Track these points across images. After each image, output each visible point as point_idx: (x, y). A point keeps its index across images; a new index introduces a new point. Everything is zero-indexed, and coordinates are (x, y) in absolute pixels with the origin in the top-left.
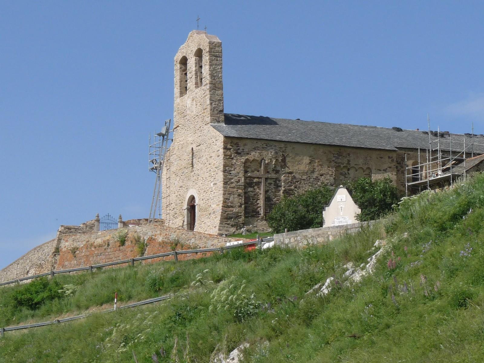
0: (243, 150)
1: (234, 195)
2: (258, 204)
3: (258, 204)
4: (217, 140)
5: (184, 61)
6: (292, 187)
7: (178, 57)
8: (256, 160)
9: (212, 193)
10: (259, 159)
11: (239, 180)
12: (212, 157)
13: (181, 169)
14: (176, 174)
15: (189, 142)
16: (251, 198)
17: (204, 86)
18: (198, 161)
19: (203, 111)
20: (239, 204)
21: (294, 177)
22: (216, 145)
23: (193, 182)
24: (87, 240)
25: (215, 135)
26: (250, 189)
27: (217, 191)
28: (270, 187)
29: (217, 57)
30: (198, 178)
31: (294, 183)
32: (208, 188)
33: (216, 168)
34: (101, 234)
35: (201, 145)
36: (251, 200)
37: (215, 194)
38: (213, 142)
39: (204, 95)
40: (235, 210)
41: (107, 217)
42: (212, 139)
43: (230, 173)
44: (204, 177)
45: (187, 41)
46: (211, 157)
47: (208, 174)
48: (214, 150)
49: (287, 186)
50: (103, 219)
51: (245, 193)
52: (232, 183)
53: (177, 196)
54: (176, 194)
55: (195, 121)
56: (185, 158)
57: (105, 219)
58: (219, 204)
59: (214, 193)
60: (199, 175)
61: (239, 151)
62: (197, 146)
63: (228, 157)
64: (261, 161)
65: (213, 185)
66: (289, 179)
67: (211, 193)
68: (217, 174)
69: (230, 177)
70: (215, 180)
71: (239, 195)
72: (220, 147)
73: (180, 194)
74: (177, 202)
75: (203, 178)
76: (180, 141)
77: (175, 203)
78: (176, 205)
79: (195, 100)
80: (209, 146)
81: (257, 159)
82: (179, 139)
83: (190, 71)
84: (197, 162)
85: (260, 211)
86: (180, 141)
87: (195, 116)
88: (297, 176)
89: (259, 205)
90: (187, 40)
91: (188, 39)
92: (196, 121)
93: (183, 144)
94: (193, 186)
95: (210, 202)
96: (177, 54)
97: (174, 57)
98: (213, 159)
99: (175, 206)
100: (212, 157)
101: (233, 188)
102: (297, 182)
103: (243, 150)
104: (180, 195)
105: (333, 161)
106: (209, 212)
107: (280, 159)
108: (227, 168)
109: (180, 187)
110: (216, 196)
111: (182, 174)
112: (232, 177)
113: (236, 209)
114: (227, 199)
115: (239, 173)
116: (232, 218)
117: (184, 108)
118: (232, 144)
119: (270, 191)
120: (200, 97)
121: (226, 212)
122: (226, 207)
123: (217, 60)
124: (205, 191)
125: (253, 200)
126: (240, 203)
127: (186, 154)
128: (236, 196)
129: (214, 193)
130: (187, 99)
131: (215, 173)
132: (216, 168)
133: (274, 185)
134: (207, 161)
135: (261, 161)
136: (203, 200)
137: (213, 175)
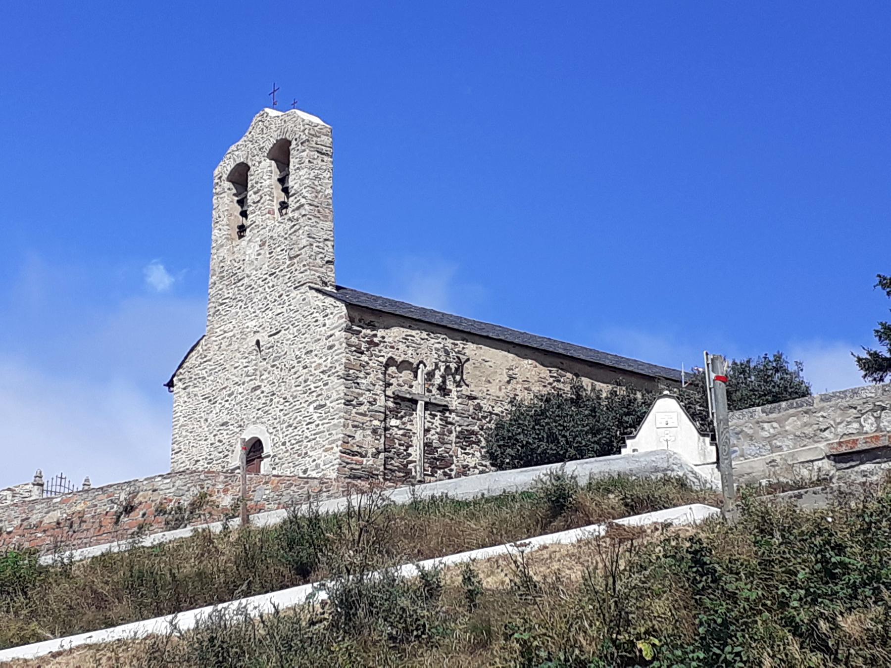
0: (383, 337)
1: (364, 429)
2: (410, 455)
3: (410, 455)
4: (327, 316)
5: (240, 177)
6: (476, 428)
7: (226, 167)
8: (408, 361)
9: (312, 426)
10: (415, 362)
11: (375, 400)
12: (311, 351)
13: (225, 388)
14: (210, 401)
15: (249, 330)
16: (396, 441)
17: (293, 211)
18: (273, 366)
19: (288, 262)
20: (374, 450)
21: (479, 408)
22: (324, 325)
23: (258, 410)
24: (24, 516)
25: (321, 304)
26: (394, 422)
27: (326, 421)
28: (433, 423)
29: (323, 154)
30: (271, 400)
31: (478, 420)
32: (299, 418)
33: (322, 372)
34: (60, 502)
35: (283, 332)
36: (397, 445)
37: (320, 427)
38: (316, 321)
39: (293, 230)
40: (368, 462)
41: (59, 480)
42: (314, 315)
43: (358, 384)
44: (288, 397)
45: (247, 134)
46: (309, 352)
47: (298, 388)
48: (319, 337)
49: (466, 424)
50: (50, 484)
51: (386, 429)
52: (361, 404)
53: (212, 444)
54: (209, 442)
55: (266, 286)
56: (236, 365)
57: (54, 483)
58: (332, 448)
59: (318, 425)
60: (274, 394)
61: (376, 340)
62: (270, 336)
63: (354, 349)
64: (418, 365)
65: (315, 408)
66: (469, 411)
67: (309, 426)
68: (325, 385)
69: (357, 390)
70: (319, 398)
71: (374, 431)
72: (336, 327)
73: (222, 439)
74: (212, 457)
75: (284, 399)
76: (225, 332)
77: (206, 458)
78: (208, 463)
79: (267, 244)
80: (303, 331)
81: (411, 360)
82: (222, 328)
83: (255, 189)
84: (270, 369)
85: (413, 470)
86: (225, 332)
87: (265, 277)
88: (486, 407)
89: (410, 458)
90: (250, 130)
91: (251, 128)
92: (270, 285)
93: (234, 336)
94: (258, 418)
95: (306, 447)
96: (221, 163)
97: (214, 170)
98: (316, 355)
99: (206, 465)
100: (311, 351)
101: (364, 415)
102: (485, 417)
103: (383, 337)
104: (220, 441)
106: (304, 468)
107: (453, 366)
108: (351, 372)
109: (222, 425)
110: (324, 432)
111: (227, 398)
112: (361, 391)
113: (368, 461)
114: (349, 436)
115: (374, 385)
117: (236, 264)
118: (361, 324)
119: (433, 432)
120: (283, 234)
121: (348, 463)
122: (349, 454)
123: (323, 161)
124: (290, 426)
125: (400, 445)
126: (376, 449)
127: (239, 355)
128: (369, 432)
129: (318, 425)
130: (249, 247)
131: (320, 383)
132: (322, 372)
133: (441, 419)
134: (299, 362)
135: (418, 365)
136: (284, 444)
137: (313, 389)
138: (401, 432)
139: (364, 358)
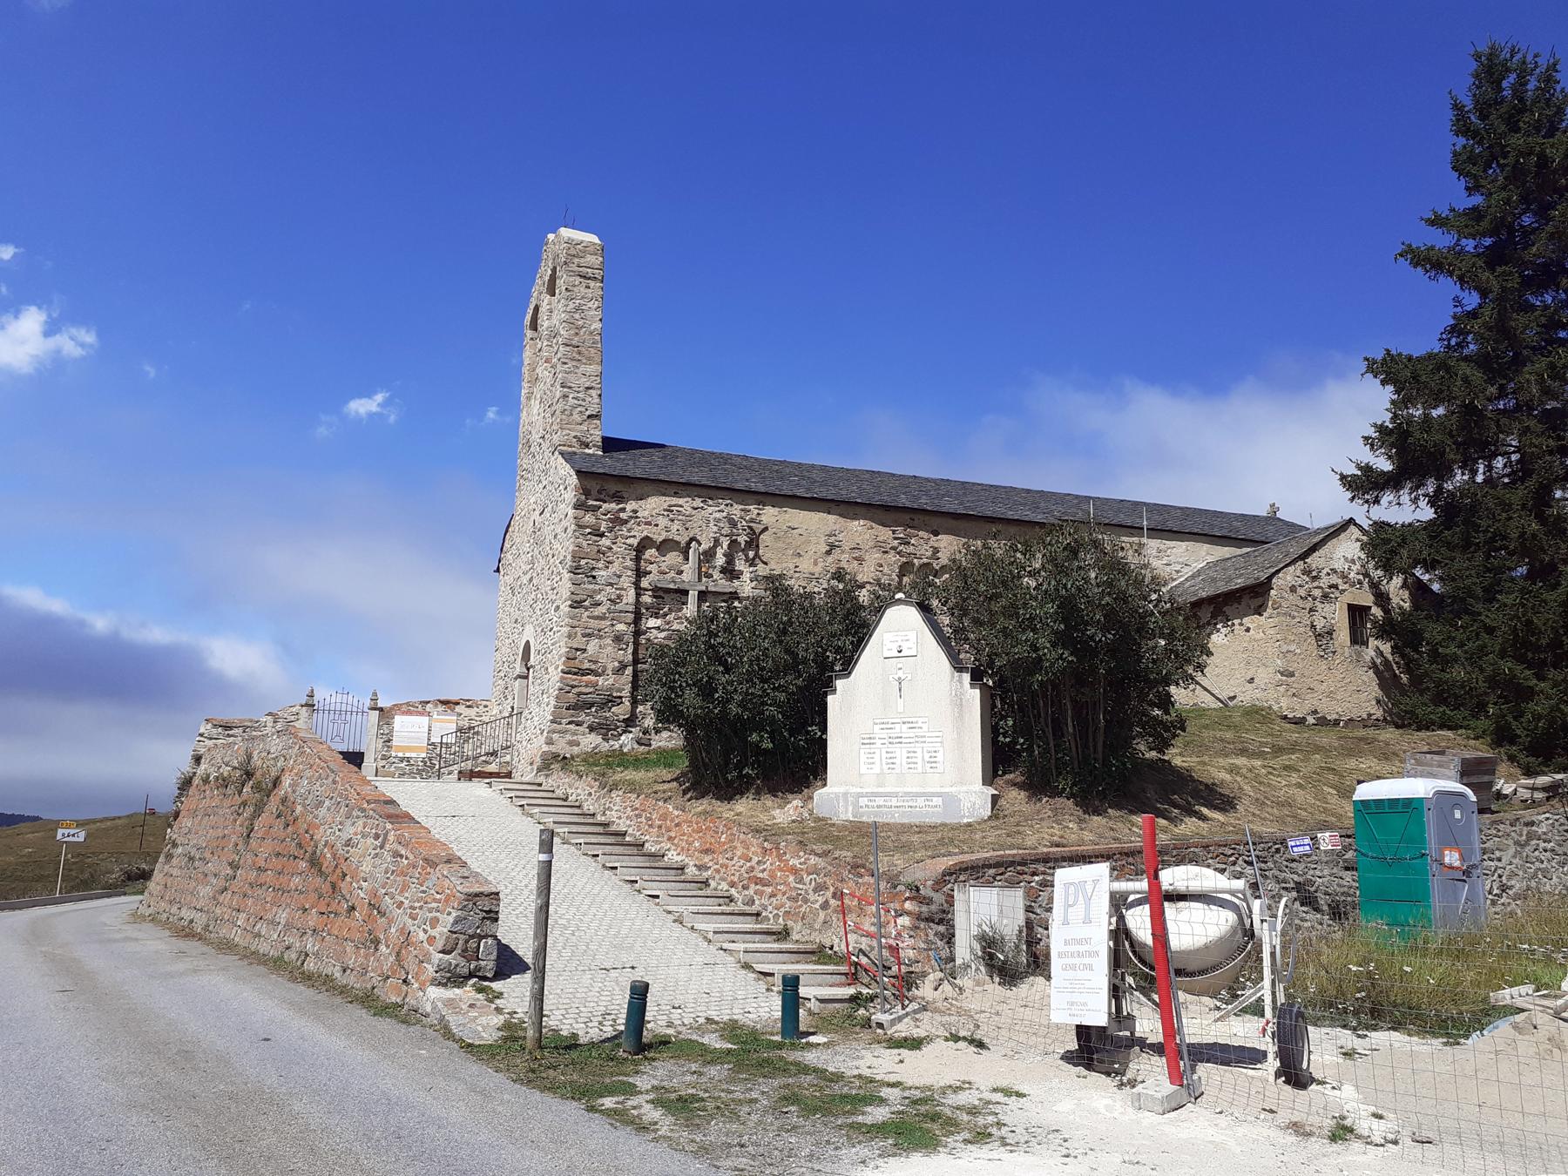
105: (894, 548)
116: (592, 705)
138: (663, 635)
139: (605, 542)
